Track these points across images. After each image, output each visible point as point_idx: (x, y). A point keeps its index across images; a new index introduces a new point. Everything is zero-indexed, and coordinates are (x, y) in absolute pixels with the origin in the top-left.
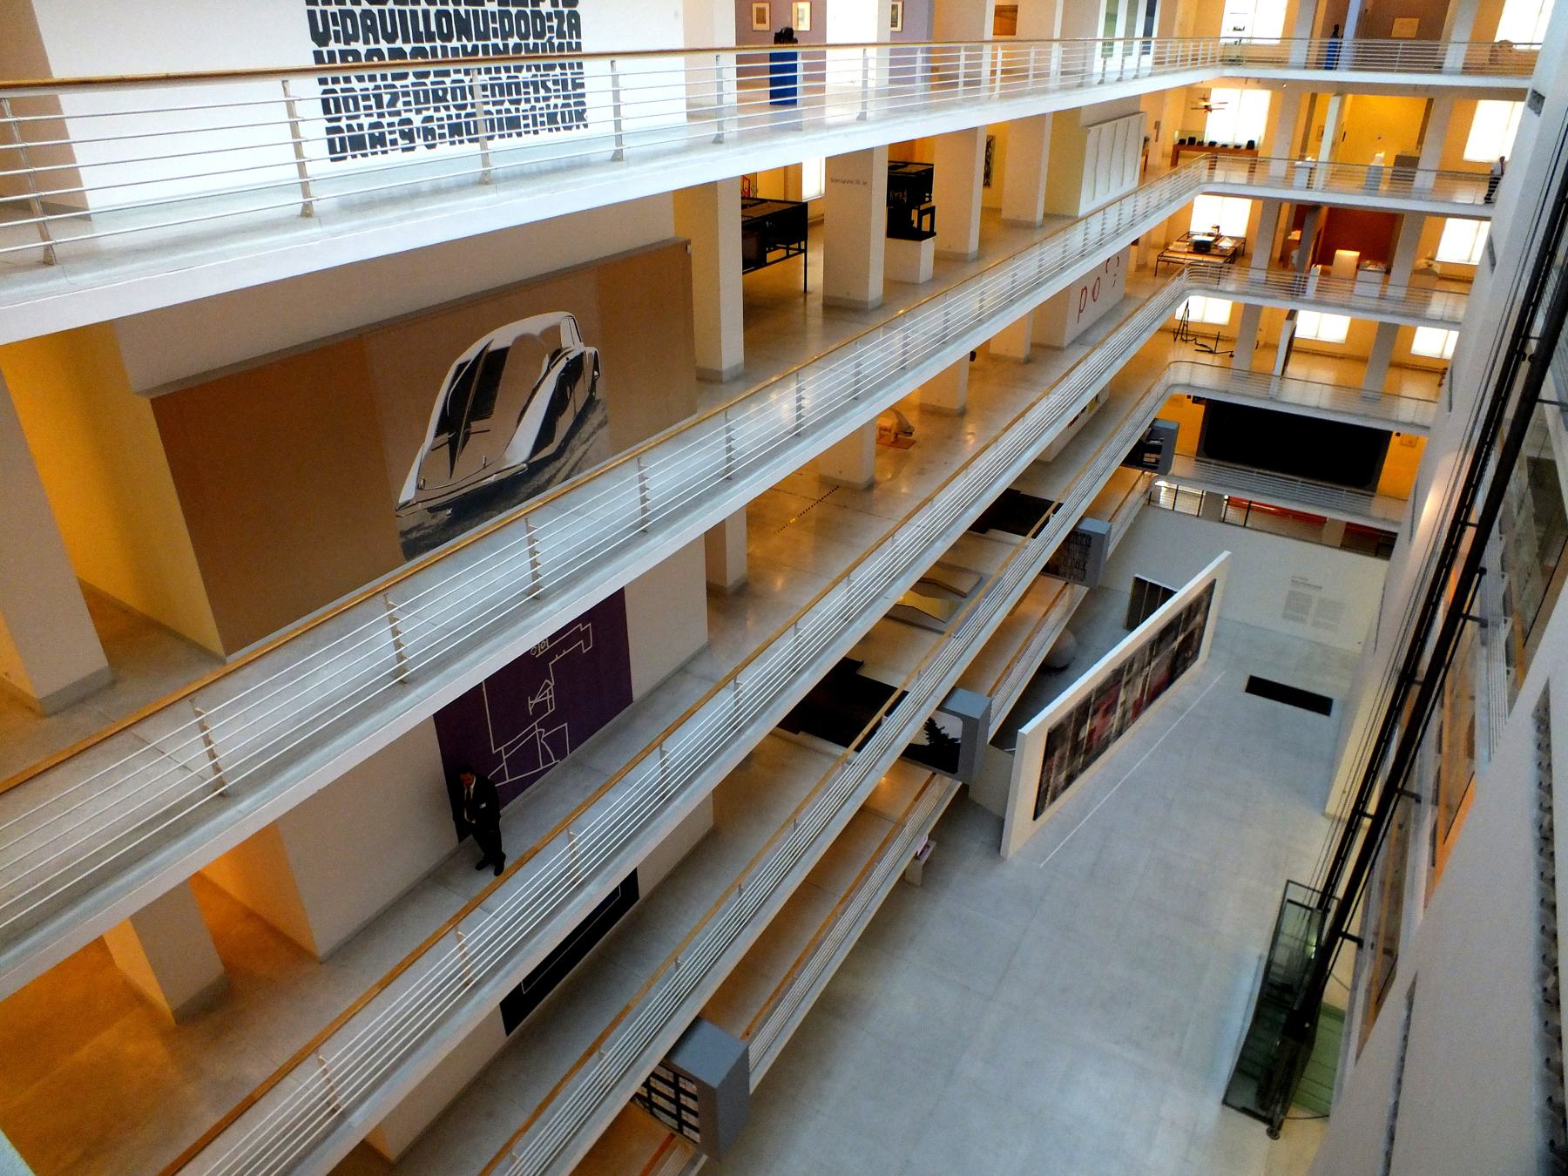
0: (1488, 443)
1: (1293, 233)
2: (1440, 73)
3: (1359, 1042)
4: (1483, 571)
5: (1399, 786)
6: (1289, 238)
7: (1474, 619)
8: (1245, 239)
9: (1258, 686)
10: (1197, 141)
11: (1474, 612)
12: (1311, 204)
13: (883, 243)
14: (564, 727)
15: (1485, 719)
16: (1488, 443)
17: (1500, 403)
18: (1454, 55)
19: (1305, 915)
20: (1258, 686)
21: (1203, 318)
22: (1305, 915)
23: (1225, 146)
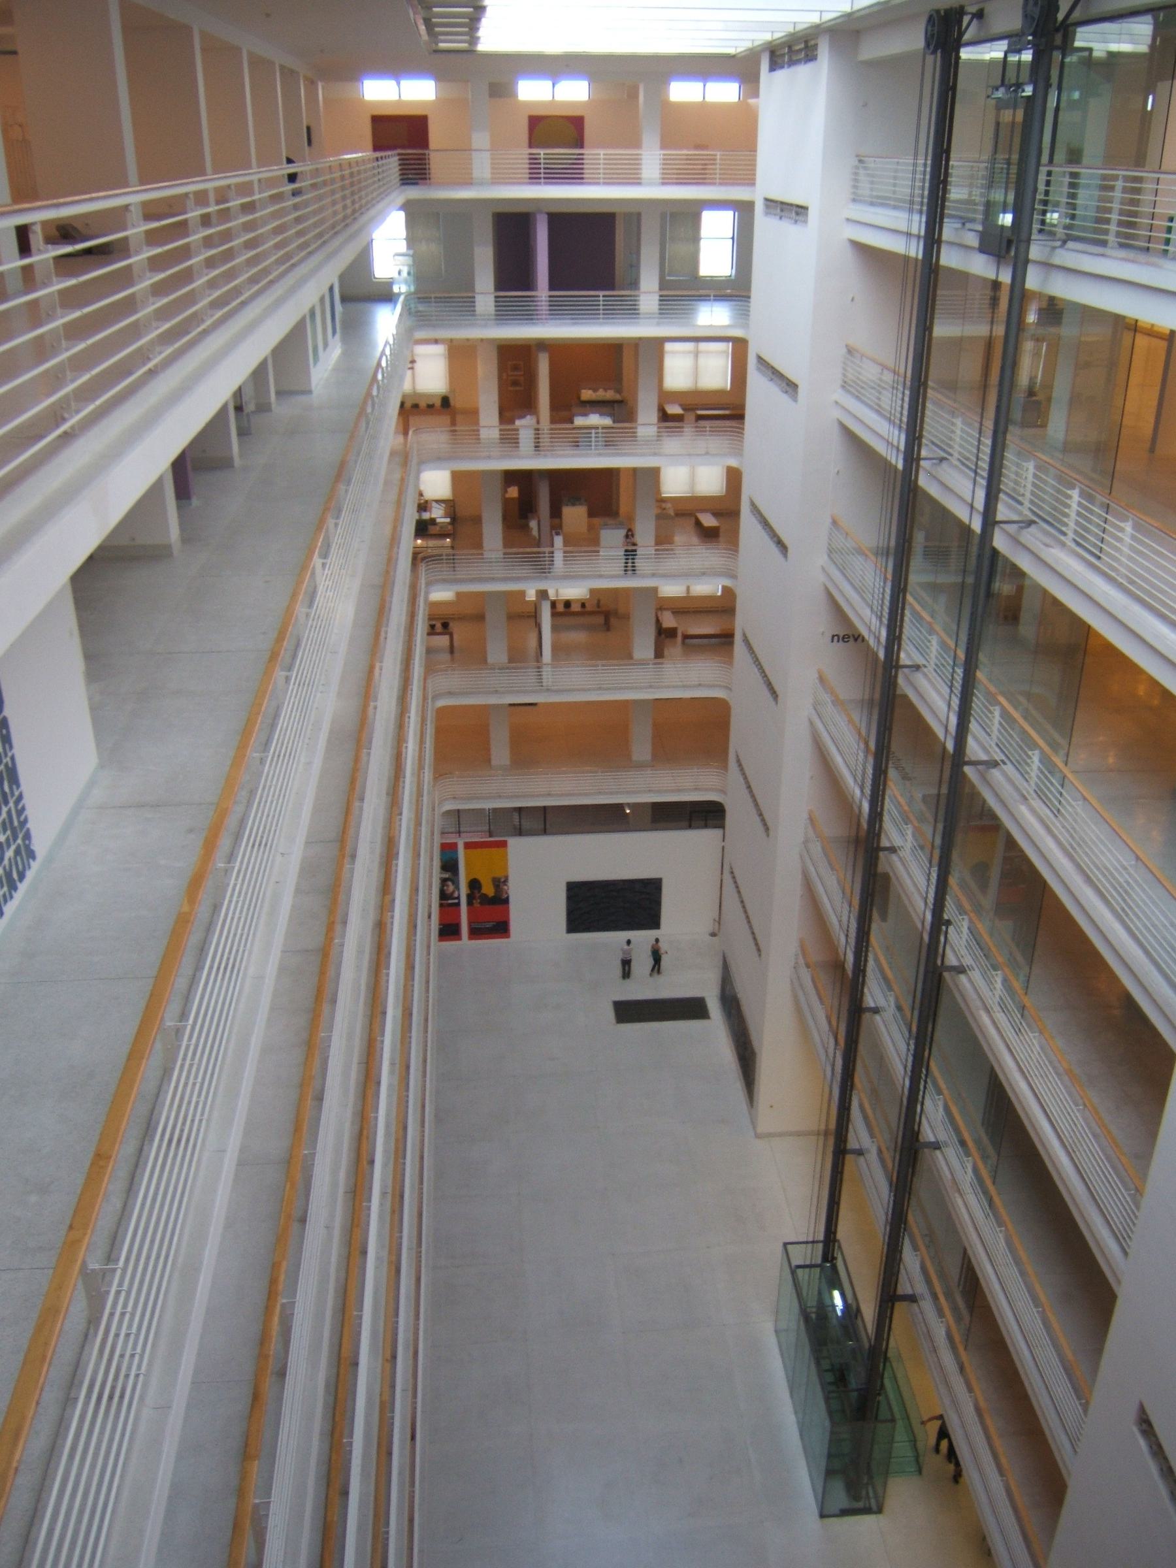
2: (639, 184)
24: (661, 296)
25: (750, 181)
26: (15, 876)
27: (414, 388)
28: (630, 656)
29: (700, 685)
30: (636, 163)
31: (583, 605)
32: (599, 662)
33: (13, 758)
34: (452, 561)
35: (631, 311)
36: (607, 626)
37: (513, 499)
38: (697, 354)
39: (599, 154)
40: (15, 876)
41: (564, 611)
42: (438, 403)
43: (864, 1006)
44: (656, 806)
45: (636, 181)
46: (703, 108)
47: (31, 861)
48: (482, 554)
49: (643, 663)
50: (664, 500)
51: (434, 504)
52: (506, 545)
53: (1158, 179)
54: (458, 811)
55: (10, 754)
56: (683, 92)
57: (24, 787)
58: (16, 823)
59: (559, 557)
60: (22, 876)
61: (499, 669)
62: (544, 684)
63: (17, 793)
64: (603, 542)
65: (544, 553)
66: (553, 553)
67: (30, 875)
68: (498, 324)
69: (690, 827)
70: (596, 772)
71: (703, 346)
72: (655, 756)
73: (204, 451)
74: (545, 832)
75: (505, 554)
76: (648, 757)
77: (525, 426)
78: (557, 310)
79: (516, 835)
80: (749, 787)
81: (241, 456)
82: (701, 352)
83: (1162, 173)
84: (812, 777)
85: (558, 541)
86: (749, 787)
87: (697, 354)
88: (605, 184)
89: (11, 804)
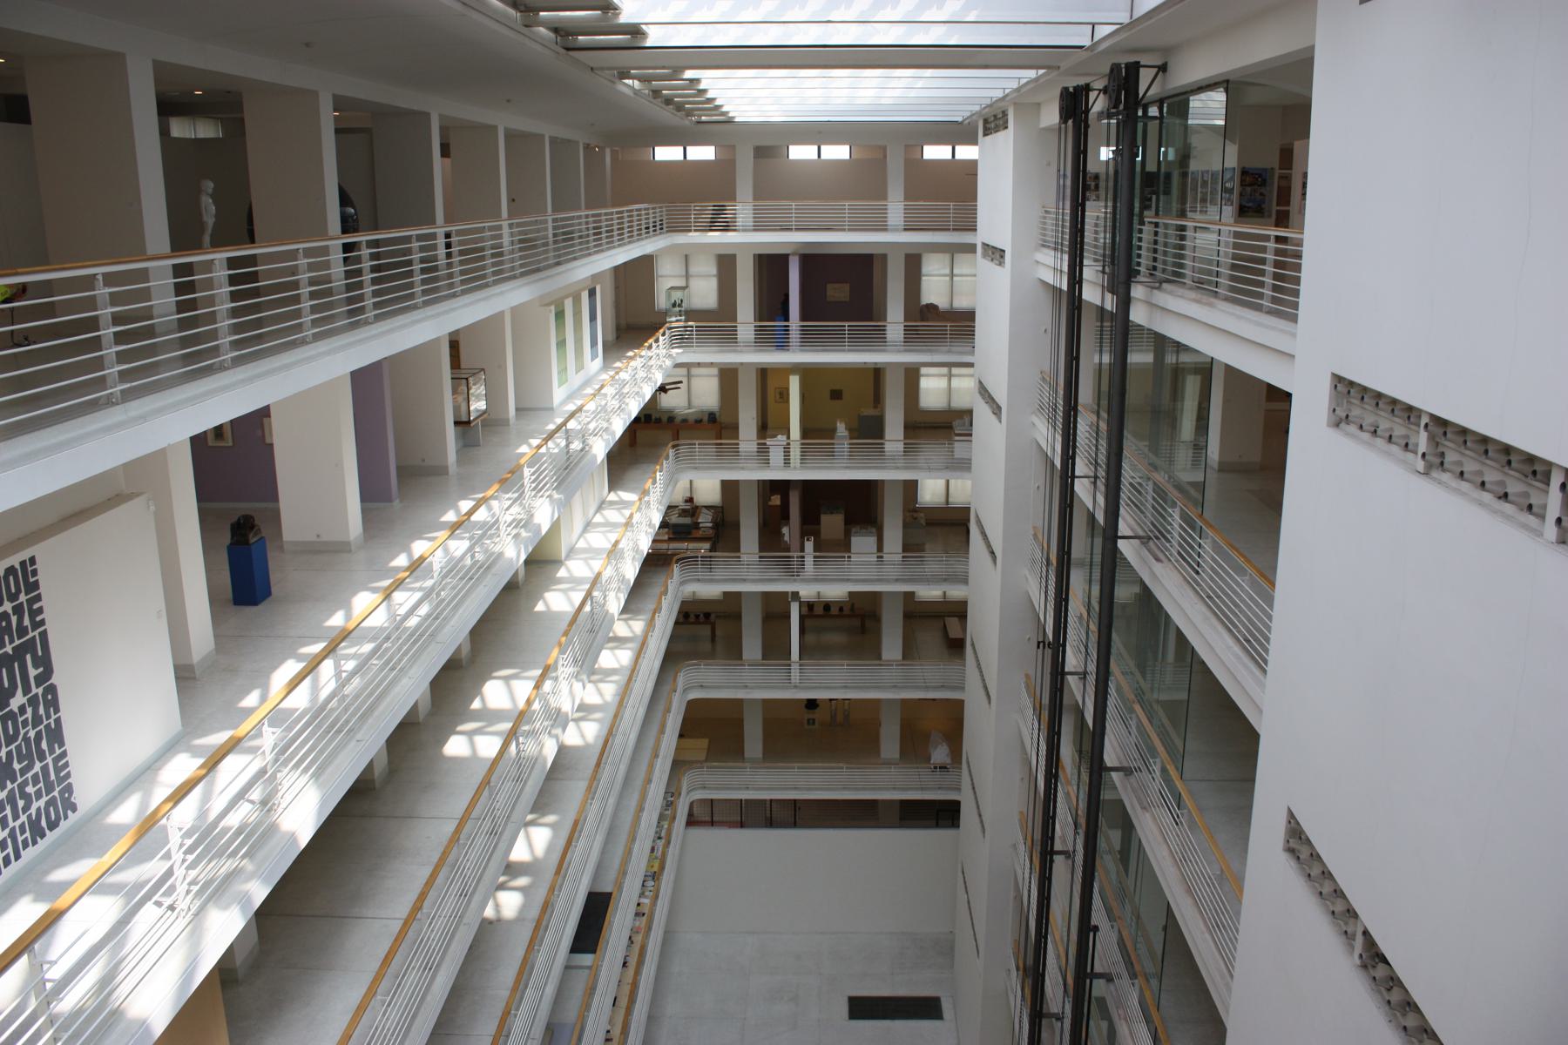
0: (1081, 205)
1: (772, 498)
2: (885, 230)
3: (1171, 909)
4: (1096, 929)
5: (1089, 970)
6: (770, 503)
7: (1100, 976)
8: (722, 507)
9: (862, 1008)
10: (653, 418)
11: (1098, 969)
12: (790, 366)
13: (345, 373)
14: (41, 788)
15: (1204, 301)
16: (1081, 205)
17: (1037, 1020)
18: (895, 324)
19: (1061, 259)
20: (862, 1008)
21: (714, 276)
22: (1061, 259)
23: (685, 421)
24: (905, 326)
25: (973, 228)
26: (44, 823)
27: (949, 405)
28: (879, 657)
29: (942, 686)
30: (884, 211)
31: (841, 609)
32: (846, 662)
33: (58, 721)
34: (708, 562)
35: (877, 337)
36: (863, 630)
37: (777, 506)
38: (950, 376)
39: (791, 205)
40: (44, 823)
41: (817, 613)
42: (665, 419)
43: (1044, 1011)
44: (905, 804)
45: (883, 228)
46: (820, 164)
47: (69, 812)
48: (739, 557)
49: (889, 664)
50: (916, 510)
51: (704, 510)
52: (761, 549)
53: (1220, 230)
54: (712, 800)
55: (54, 717)
56: (801, 152)
57: (68, 746)
58: (53, 777)
59: (809, 560)
60: (53, 825)
61: (749, 665)
62: (793, 681)
63: (58, 752)
64: (853, 549)
65: (793, 557)
66: (803, 557)
67: (64, 825)
68: (802, 351)
69: (937, 826)
70: (842, 768)
71: (955, 371)
72: (903, 753)
73: (424, 460)
74: (795, 825)
75: (760, 557)
76: (897, 756)
77: (776, 444)
78: (810, 339)
79: (766, 827)
80: (974, 788)
81: (460, 461)
82: (693, 376)
83: (1222, 225)
84: (1022, 779)
85: (809, 546)
86: (974, 788)
87: (950, 376)
88: (849, 230)
89: (49, 760)
